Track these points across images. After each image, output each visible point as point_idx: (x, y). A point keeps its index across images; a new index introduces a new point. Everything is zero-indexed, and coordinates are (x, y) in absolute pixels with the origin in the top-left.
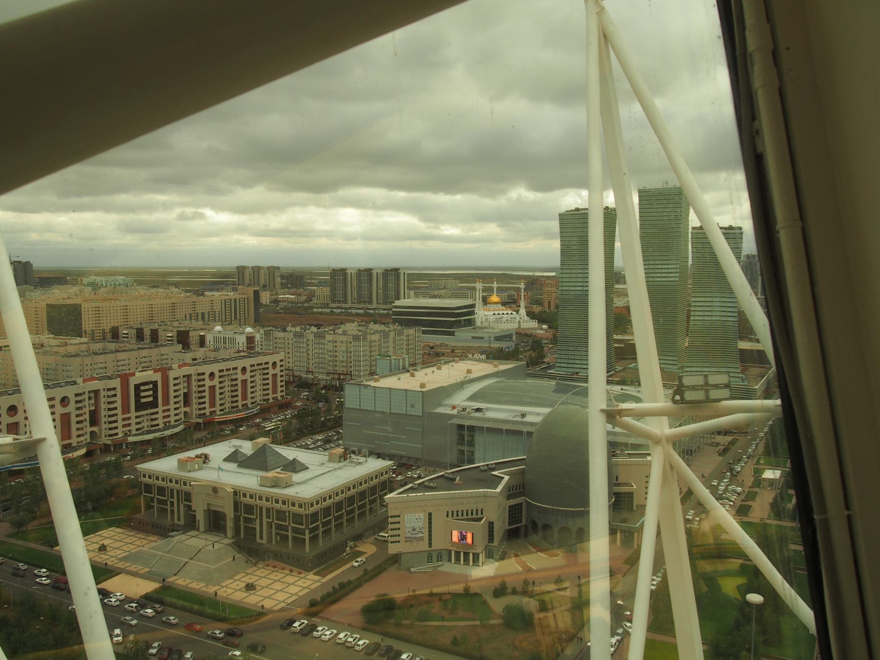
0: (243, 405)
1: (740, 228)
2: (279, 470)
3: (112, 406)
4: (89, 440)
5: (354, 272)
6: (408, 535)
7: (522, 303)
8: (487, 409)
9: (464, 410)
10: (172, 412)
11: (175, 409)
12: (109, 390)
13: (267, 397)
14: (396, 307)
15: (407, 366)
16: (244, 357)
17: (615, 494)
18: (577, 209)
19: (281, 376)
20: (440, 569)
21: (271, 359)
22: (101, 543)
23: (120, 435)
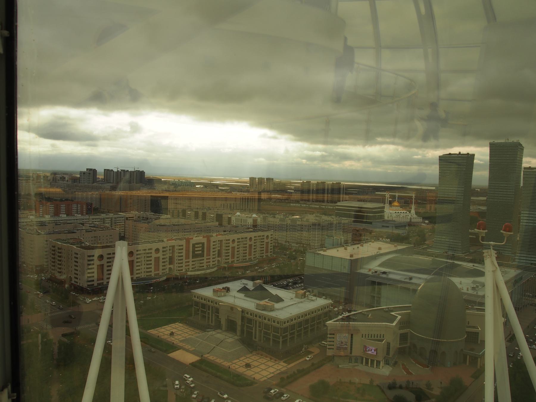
2: (267, 300)
5: (330, 187)
6: (338, 346)
8: (390, 273)
9: (376, 272)
11: (213, 258)
14: (338, 206)
17: (467, 332)
19: (271, 243)
20: (356, 368)
23: (184, 271)
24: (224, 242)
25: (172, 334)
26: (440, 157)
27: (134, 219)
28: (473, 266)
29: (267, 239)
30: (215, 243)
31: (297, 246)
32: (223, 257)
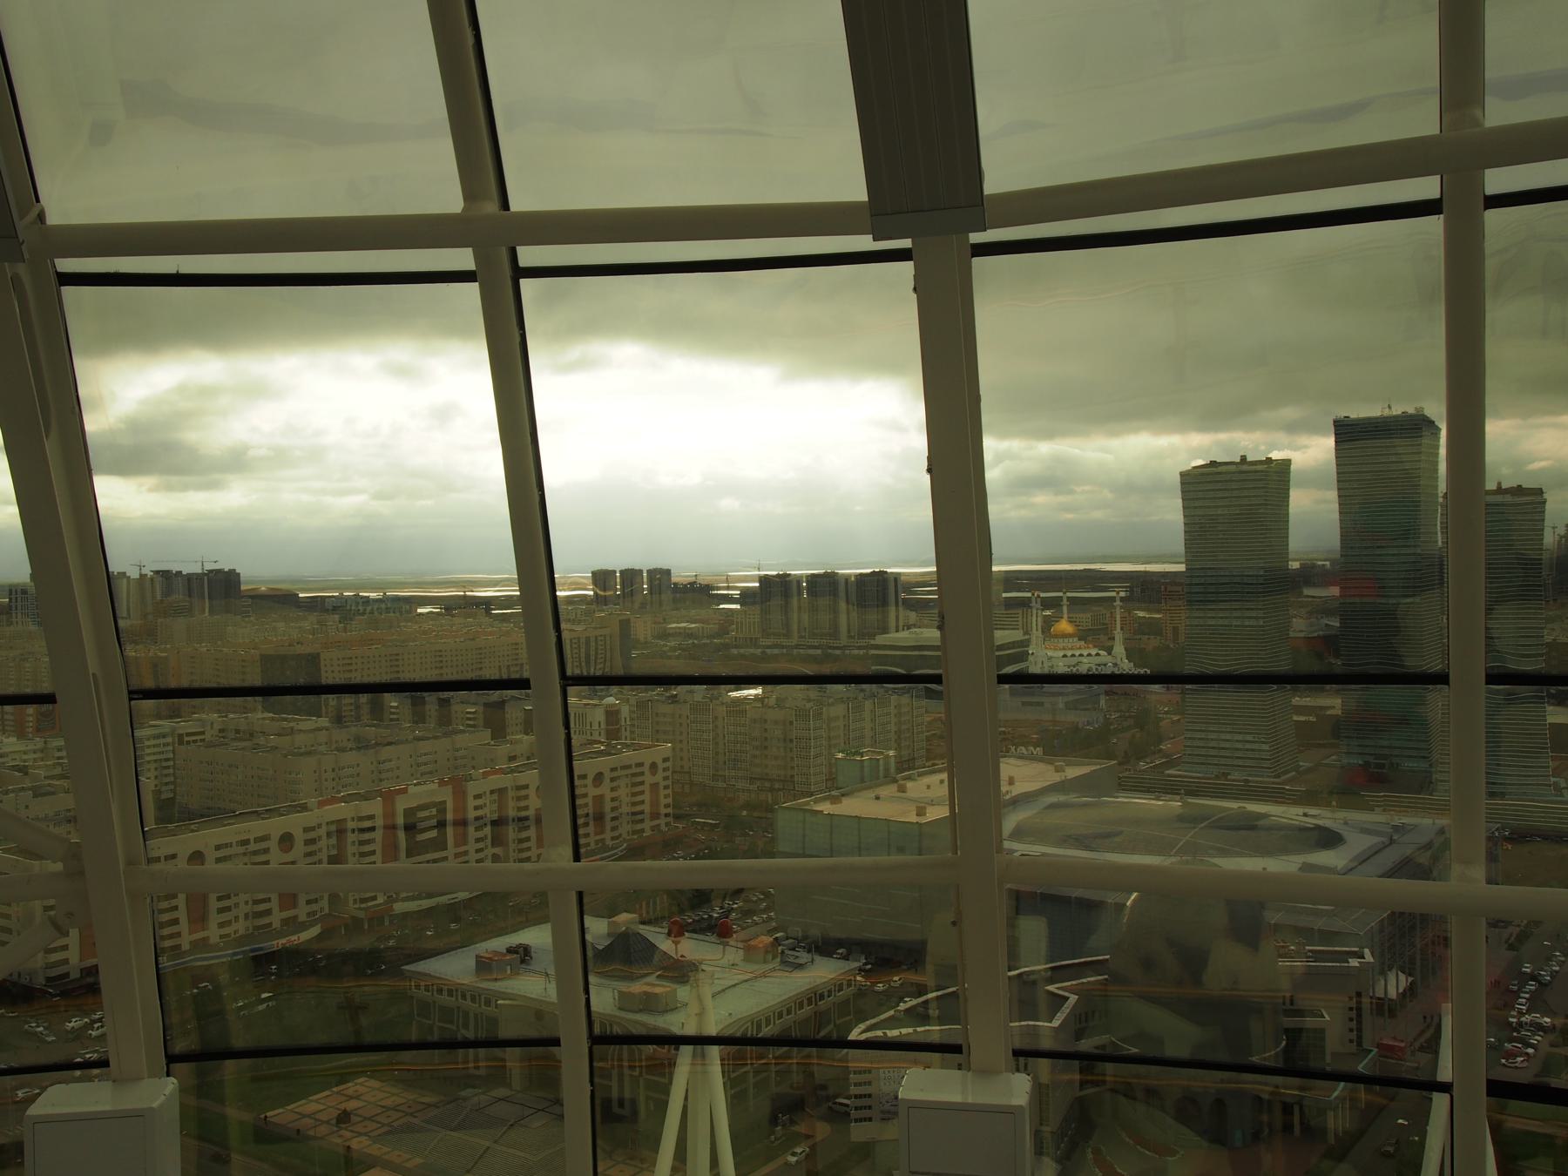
0: (597, 842)
1: (1540, 492)
2: (652, 979)
3: (367, 848)
4: (327, 911)
7: (1118, 635)
10: (473, 856)
11: (478, 851)
12: (361, 819)
13: (639, 827)
14: (877, 647)
15: (893, 770)
16: (601, 753)
17: (1287, 1031)
18: (1213, 464)
19: (666, 787)
21: (646, 756)
22: (342, 1107)
23: (380, 900)
24: (511, 794)
25: (344, 1118)
26: (1182, 474)
27: (207, 737)
28: (1305, 815)
29: (654, 774)
30: (479, 802)
31: (754, 787)
32: (512, 846)
